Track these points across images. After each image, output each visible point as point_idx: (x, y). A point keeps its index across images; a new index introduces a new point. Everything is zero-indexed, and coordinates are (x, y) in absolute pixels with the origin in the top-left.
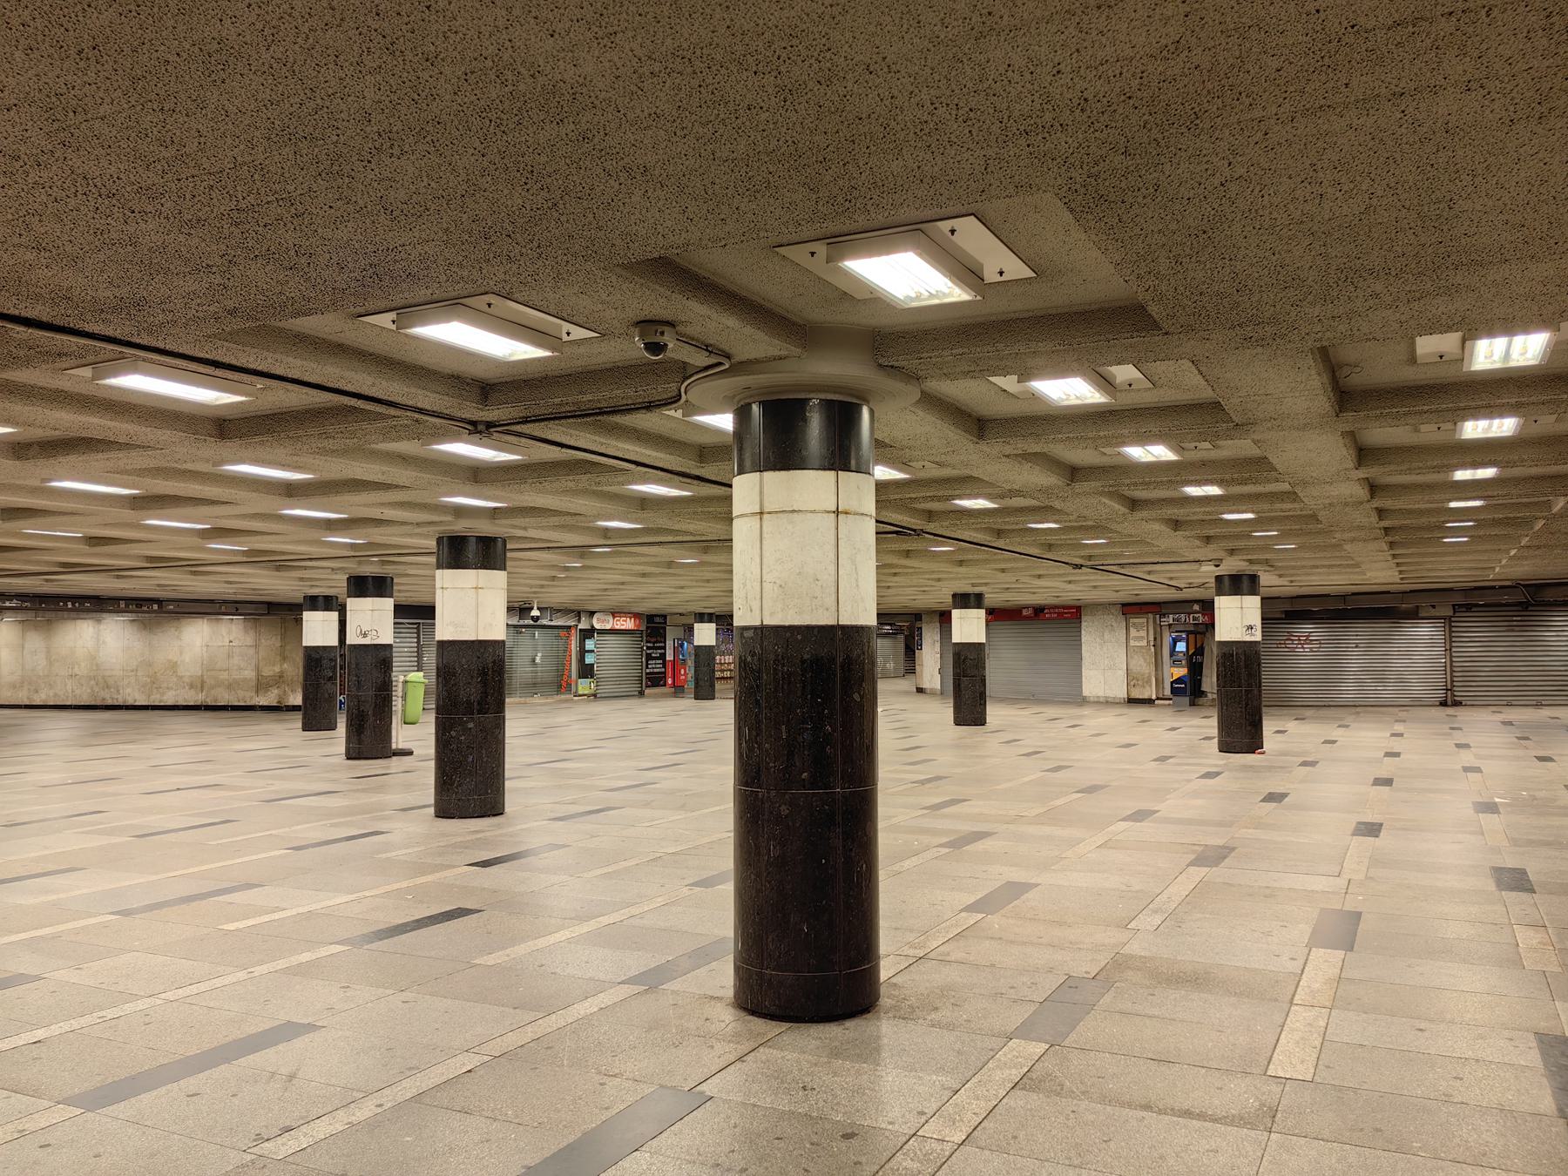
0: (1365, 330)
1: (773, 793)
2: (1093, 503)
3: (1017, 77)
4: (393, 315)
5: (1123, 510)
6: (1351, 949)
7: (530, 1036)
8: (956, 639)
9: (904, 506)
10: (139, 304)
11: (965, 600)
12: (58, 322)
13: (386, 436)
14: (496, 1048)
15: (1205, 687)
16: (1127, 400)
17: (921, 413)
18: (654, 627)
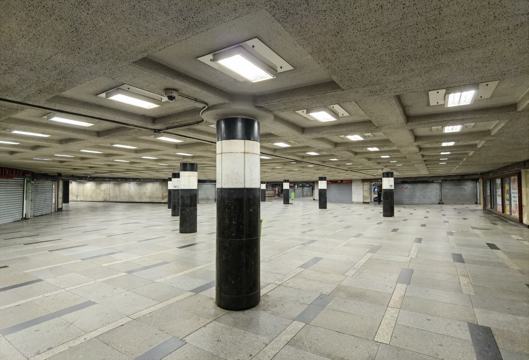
5: (352, 155)
11: (322, 179)
16: (342, 121)
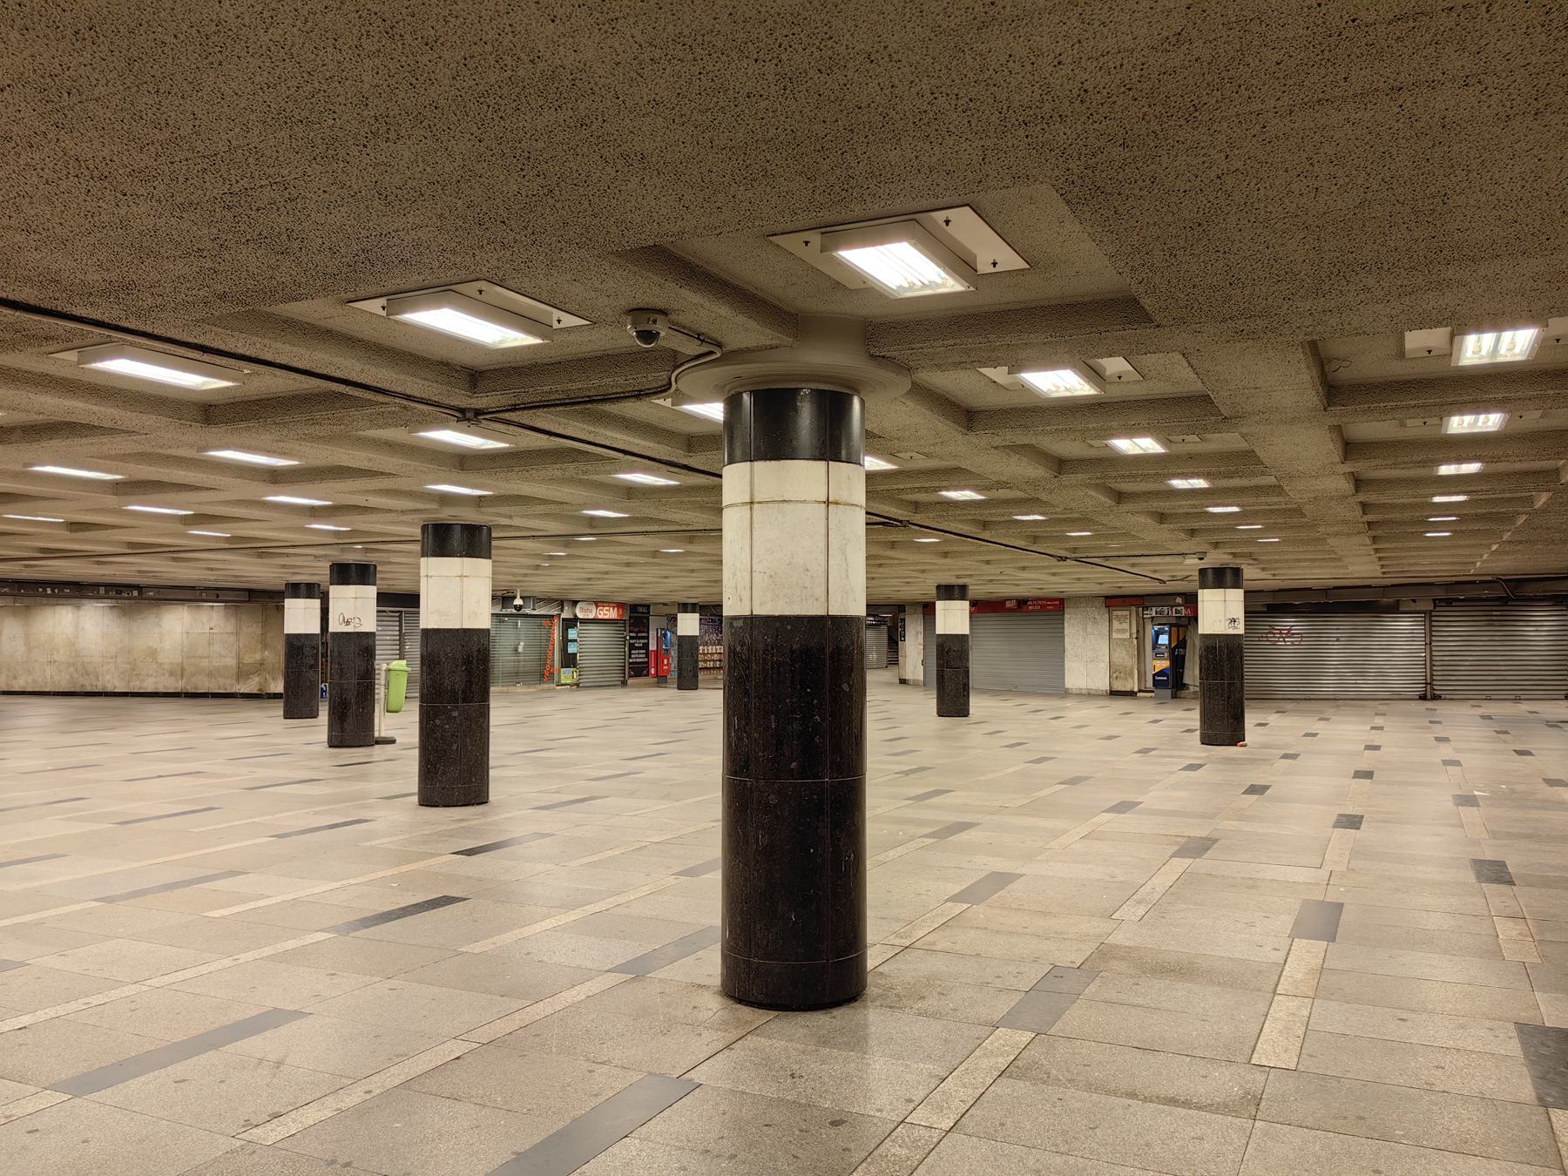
0: (1355, 324)
1: (762, 782)
2: (1080, 495)
3: (1016, 67)
4: (383, 301)
6: (1333, 939)
7: (518, 1023)
8: (940, 630)
9: (888, 497)
10: (128, 287)
11: (950, 592)
12: (46, 305)
13: (374, 424)
14: (484, 1035)
15: (1186, 680)
16: (1116, 392)
17: (909, 403)
18: (637, 617)
